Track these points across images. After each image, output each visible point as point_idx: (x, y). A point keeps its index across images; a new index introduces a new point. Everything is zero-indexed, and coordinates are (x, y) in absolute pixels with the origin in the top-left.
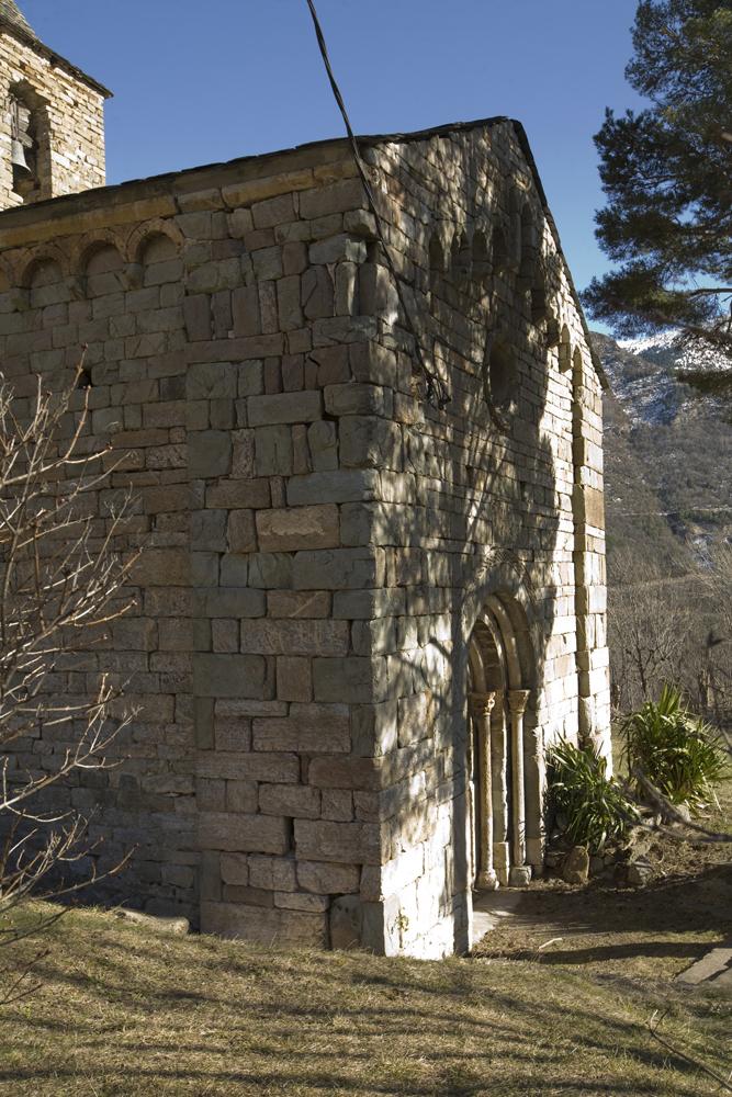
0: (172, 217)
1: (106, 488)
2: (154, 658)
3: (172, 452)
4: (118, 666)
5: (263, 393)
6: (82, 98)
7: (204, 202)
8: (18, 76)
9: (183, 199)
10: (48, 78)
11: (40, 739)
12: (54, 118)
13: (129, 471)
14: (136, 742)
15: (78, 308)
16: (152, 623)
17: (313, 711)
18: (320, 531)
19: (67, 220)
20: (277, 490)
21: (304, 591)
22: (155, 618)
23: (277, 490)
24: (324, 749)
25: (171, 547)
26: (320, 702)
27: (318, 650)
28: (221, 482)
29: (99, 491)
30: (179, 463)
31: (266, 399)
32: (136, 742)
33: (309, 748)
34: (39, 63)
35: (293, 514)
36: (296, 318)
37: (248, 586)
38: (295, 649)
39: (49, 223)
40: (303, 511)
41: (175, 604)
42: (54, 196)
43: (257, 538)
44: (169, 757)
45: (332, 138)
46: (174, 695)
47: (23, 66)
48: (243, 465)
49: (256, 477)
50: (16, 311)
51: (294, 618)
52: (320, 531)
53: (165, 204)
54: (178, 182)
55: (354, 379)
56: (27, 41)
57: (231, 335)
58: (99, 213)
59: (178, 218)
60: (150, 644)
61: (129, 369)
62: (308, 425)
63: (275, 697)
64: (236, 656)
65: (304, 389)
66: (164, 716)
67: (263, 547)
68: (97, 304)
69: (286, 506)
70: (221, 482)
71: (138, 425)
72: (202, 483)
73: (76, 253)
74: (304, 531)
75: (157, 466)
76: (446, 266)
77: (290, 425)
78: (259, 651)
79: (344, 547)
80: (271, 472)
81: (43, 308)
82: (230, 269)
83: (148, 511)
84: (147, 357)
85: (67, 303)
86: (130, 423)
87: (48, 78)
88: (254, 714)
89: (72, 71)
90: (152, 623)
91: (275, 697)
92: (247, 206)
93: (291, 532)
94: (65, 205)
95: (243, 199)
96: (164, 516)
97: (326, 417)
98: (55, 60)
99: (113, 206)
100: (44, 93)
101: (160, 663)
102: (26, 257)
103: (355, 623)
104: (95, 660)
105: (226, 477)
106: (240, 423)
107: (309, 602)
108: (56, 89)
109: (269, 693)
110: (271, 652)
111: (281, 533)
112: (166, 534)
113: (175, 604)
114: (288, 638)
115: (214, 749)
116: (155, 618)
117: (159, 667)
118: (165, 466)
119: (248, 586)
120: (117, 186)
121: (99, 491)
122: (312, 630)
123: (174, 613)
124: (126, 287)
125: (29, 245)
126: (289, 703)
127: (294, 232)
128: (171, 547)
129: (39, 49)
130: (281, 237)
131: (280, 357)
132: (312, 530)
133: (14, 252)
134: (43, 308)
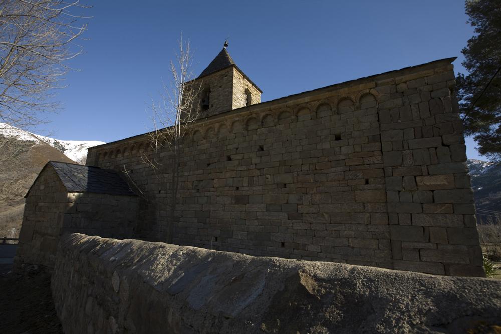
0: (374, 88)
1: (347, 171)
2: (369, 227)
3: (374, 158)
4: (354, 229)
5: (415, 138)
6: (257, 93)
7: (388, 82)
8: (246, 87)
9: (379, 82)
10: (252, 88)
11: (321, 252)
12: (252, 97)
13: (356, 165)
14: (361, 255)
17: (450, 247)
20: (424, 169)
21: (440, 204)
22: (370, 213)
23: (424, 169)
24: (456, 262)
26: (452, 245)
28: (399, 167)
29: (344, 172)
30: (377, 162)
32: (361, 255)
34: (250, 85)
37: (413, 202)
39: (327, 93)
41: (378, 209)
44: (377, 261)
45: (431, 61)
46: (378, 239)
47: (247, 85)
50: (312, 119)
51: (436, 214)
53: (372, 84)
54: (338, 87)
55: (455, 132)
56: (249, 80)
57: (399, 121)
59: (376, 88)
60: (367, 222)
62: (436, 148)
63: (429, 241)
64: (411, 227)
65: (433, 136)
66: (374, 247)
68: (342, 116)
70: (399, 167)
71: (360, 151)
72: (391, 168)
73: (336, 101)
74: (439, 183)
75: (368, 163)
76: (471, 95)
77: (428, 148)
78: (422, 225)
79: (457, 188)
81: (321, 118)
82: (399, 101)
84: (363, 130)
85: (330, 116)
86: (357, 150)
87: (252, 88)
88: (421, 248)
89: (256, 87)
90: (368, 215)
91: (429, 241)
92: (405, 82)
98: (253, 85)
99: (352, 86)
100: (251, 91)
102: (317, 103)
104: (344, 226)
105: (401, 166)
106: (405, 148)
107: (443, 208)
108: (253, 90)
109: (428, 240)
110: (427, 225)
111: (428, 184)
112: (373, 185)
113: (378, 209)
114: (435, 220)
115: (402, 259)
116: (370, 213)
117: (372, 230)
118: (372, 163)
119: (413, 202)
121: (344, 172)
123: (378, 211)
124: (354, 110)
125: (318, 100)
128: (376, 189)
130: (420, 90)
131: (421, 127)
132: (442, 183)
133: (312, 102)
134: (321, 118)
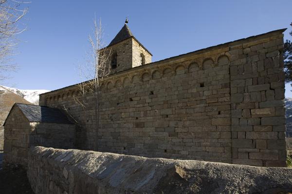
9: (232, 47)
15: (200, 72)
16: (219, 133)
17: (267, 151)
18: (270, 113)
19: (201, 54)
20: (257, 105)
23: (257, 105)
24: (271, 159)
25: (224, 117)
27: (269, 138)
31: (254, 86)
33: (265, 159)
35: (262, 110)
36: (263, 68)
38: (262, 138)
40: (265, 109)
42: (133, 67)
43: (251, 114)
48: (247, 100)
49: (251, 102)
52: (270, 113)
53: (227, 49)
56: (143, 47)
57: (243, 74)
58: (209, 52)
61: (214, 83)
62: (266, 91)
67: (252, 117)
68: (205, 71)
69: (259, 108)
80: (255, 101)
82: (244, 60)
83: (219, 110)
89: (148, 52)
91: (255, 148)
92: (250, 47)
93: (261, 113)
94: (200, 52)
95: (248, 46)
96: (223, 111)
97: (271, 89)
98: (146, 50)
101: (220, 141)
102: (189, 63)
103: (280, 133)
106: (246, 91)
108: (145, 54)
120: (215, 46)
122: (267, 134)
126: (260, 149)
127: (263, 51)
129: (144, 48)
